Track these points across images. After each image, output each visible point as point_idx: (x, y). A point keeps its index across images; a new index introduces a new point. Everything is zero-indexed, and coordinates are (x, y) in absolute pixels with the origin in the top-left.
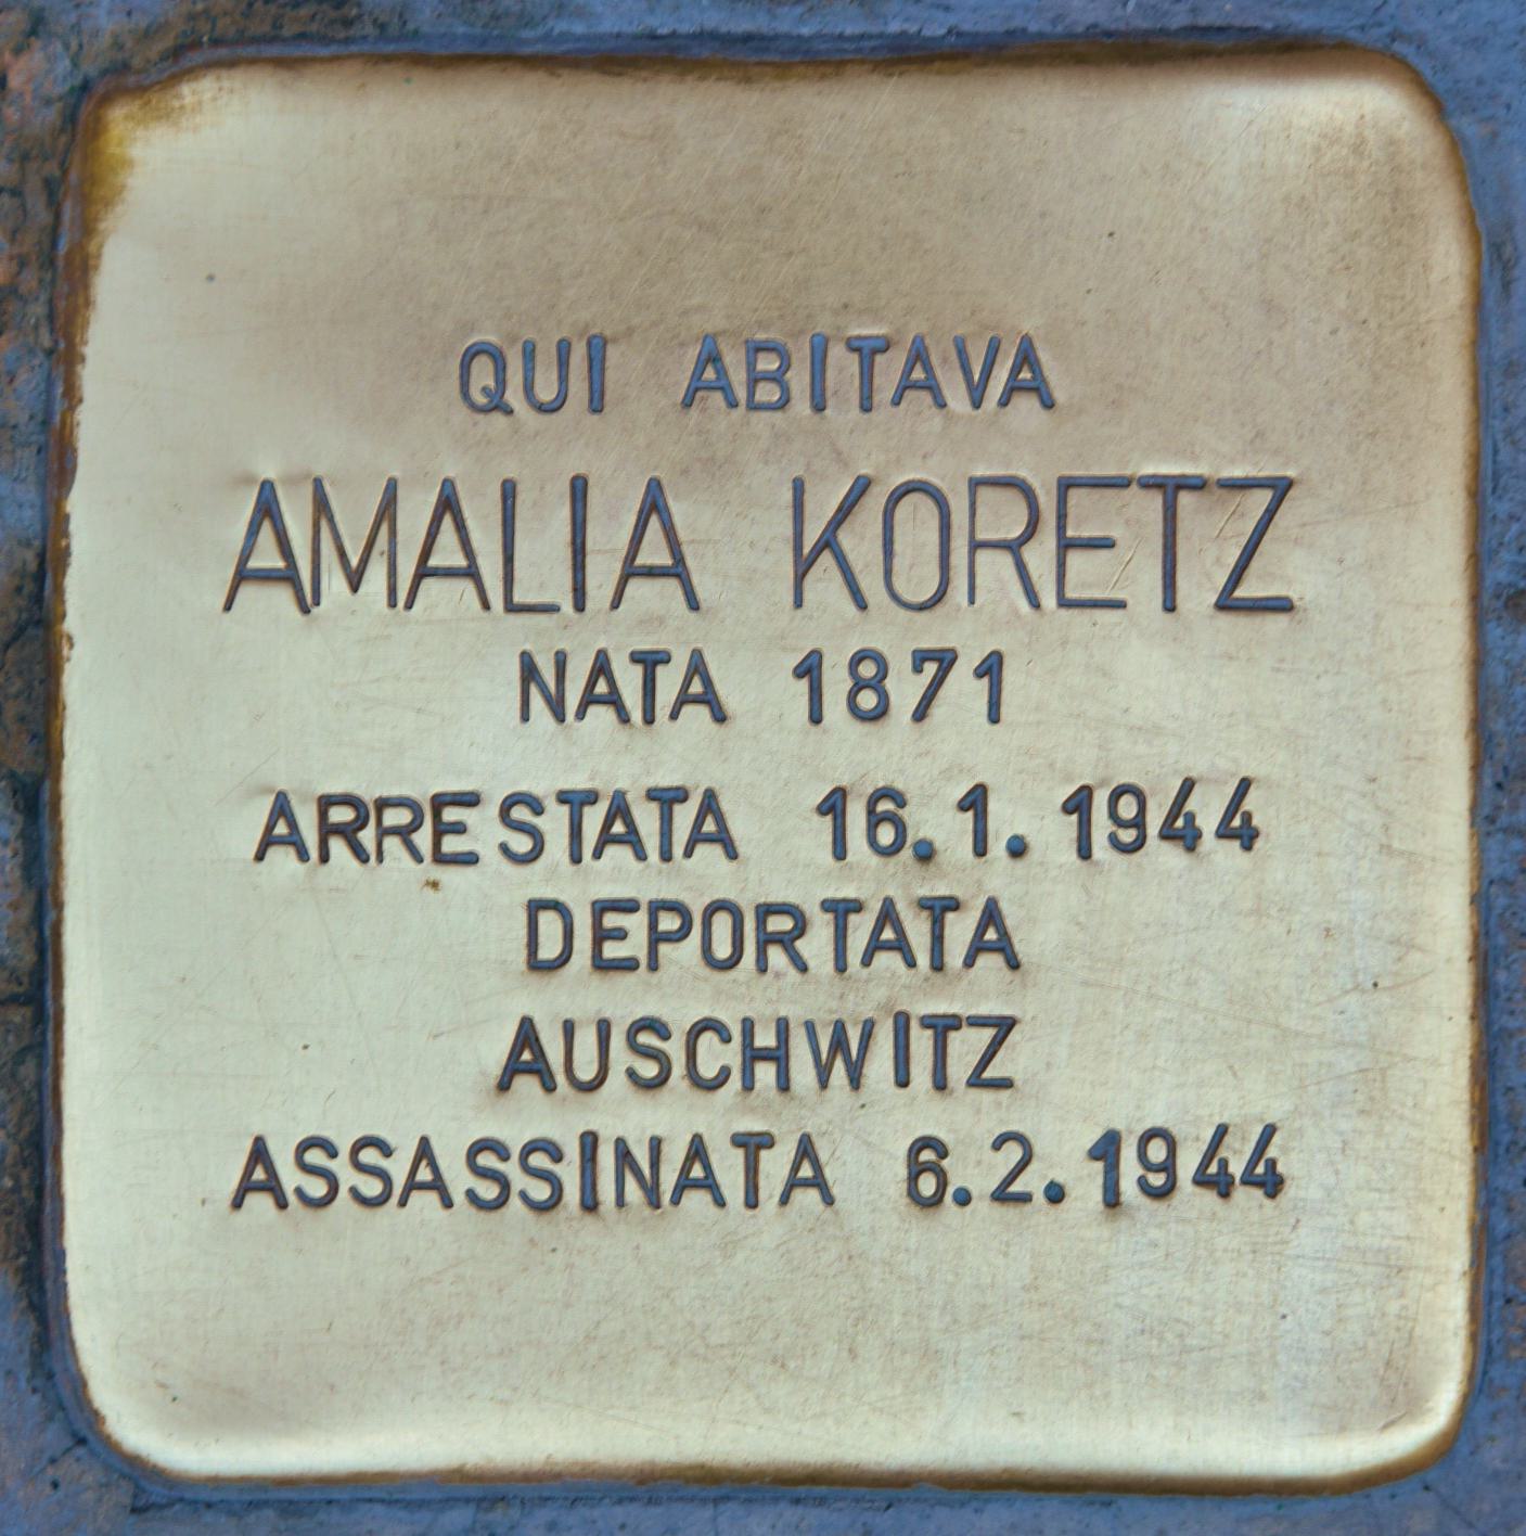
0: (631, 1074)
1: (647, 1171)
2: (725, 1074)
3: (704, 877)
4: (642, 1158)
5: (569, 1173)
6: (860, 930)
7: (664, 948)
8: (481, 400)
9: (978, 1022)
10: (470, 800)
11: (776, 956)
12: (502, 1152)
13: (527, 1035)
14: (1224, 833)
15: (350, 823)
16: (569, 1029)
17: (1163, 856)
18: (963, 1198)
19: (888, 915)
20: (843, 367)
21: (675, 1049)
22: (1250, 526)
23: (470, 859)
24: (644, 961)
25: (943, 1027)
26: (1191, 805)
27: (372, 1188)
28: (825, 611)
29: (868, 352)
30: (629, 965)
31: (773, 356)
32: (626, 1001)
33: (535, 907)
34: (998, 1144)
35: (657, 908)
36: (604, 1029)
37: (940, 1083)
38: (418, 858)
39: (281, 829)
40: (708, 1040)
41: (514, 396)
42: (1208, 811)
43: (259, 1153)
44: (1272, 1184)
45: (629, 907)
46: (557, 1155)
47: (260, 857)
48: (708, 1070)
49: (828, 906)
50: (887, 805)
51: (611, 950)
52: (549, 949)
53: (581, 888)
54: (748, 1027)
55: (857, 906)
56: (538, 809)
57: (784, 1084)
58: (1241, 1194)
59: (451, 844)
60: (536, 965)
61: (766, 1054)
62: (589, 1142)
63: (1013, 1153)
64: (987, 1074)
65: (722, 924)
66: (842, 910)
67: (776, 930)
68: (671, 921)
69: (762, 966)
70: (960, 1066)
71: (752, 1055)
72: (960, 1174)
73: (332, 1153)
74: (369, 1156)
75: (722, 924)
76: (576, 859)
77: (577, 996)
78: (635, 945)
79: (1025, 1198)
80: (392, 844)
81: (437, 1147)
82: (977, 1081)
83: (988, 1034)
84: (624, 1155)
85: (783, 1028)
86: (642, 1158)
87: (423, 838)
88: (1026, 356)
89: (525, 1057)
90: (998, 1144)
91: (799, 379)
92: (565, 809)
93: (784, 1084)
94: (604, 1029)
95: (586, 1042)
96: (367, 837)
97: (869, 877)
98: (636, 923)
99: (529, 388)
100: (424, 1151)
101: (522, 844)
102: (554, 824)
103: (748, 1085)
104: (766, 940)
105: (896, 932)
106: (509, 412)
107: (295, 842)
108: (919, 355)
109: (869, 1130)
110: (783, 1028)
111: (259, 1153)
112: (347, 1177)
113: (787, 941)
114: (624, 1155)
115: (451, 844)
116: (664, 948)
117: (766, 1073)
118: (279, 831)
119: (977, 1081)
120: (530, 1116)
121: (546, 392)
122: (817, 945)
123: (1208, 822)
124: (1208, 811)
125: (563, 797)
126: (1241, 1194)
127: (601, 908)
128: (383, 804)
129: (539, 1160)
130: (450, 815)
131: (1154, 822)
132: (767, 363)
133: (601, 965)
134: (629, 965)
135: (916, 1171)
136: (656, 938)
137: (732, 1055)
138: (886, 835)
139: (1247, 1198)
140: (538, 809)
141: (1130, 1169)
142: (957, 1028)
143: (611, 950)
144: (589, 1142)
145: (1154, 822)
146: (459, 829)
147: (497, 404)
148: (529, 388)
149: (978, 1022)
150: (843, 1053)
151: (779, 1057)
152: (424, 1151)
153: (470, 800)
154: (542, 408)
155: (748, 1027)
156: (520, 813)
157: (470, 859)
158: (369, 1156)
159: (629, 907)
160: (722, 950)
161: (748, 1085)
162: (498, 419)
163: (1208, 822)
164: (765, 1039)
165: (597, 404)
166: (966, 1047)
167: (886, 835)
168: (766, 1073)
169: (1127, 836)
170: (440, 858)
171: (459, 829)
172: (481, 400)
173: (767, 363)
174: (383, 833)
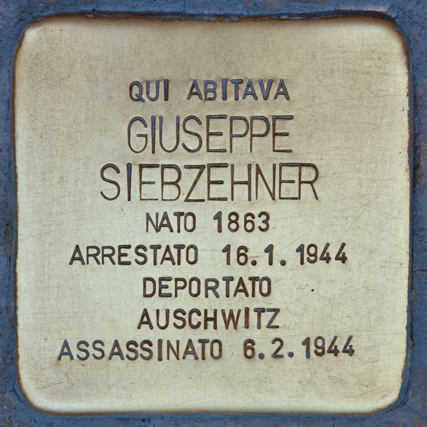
0: (175, 325)
1: (175, 349)
2: (199, 324)
3: (185, 271)
4: (174, 346)
5: (155, 349)
6: (233, 285)
7: (179, 291)
8: (135, 97)
9: (269, 310)
10: (129, 247)
11: (210, 292)
12: (135, 344)
13: (145, 313)
14: (337, 258)
15: (99, 254)
16: (158, 312)
17: (321, 263)
18: (262, 356)
19: (241, 281)
20: (231, 88)
21: (186, 317)
22: (267, 181)
23: (128, 263)
24: (173, 295)
25: (260, 311)
26: (328, 250)
27: (99, 354)
28: (118, 218)
29: (237, 83)
30: (169, 295)
31: (212, 85)
32: (172, 305)
33: (146, 279)
34: (274, 341)
35: (177, 280)
36: (167, 312)
37: (259, 327)
38: (114, 263)
39: (77, 255)
40: (194, 315)
41: (144, 96)
42: (333, 252)
43: (66, 344)
44: (351, 352)
45: (169, 279)
46: (150, 344)
47: (71, 263)
48: (195, 323)
49: (224, 279)
50: (243, 251)
51: (164, 291)
52: (149, 291)
53: (156, 273)
54: (206, 311)
55: (232, 279)
56: (145, 250)
57: (215, 327)
58: (341, 355)
59: (123, 259)
60: (145, 296)
61: (210, 319)
62: (160, 342)
63: (278, 344)
64: (272, 324)
65: (194, 283)
66: (228, 280)
67: (211, 286)
68: (183, 283)
69: (207, 296)
70: (264, 323)
71: (207, 319)
72: (258, 349)
73: (87, 345)
74: (98, 345)
75: (194, 283)
76: (155, 264)
77: (156, 304)
78: (171, 290)
79: (282, 356)
80: (107, 259)
81: (120, 343)
82: (269, 326)
83: (272, 313)
84: (169, 345)
85: (215, 312)
86: (174, 346)
87: (115, 258)
88: (282, 85)
89: (145, 319)
90: (274, 341)
91: (219, 91)
92: (153, 250)
93: (215, 327)
94: (167, 312)
95: (163, 315)
96: (99, 257)
97: (238, 272)
98: (171, 284)
99: (148, 93)
100: (116, 344)
101: (141, 259)
102: (150, 253)
103: (206, 328)
104: (207, 288)
105: (243, 287)
106: (143, 101)
107: (81, 259)
108: (250, 85)
109: (233, 340)
110: (215, 312)
111: (66, 344)
112: (91, 350)
113: (214, 289)
114: (169, 345)
115: (123, 259)
116: (179, 291)
117: (211, 324)
118: (77, 257)
119: (269, 326)
120: (145, 333)
121: (153, 95)
122: (221, 290)
123: (333, 256)
124: (333, 252)
125: (152, 247)
126: (341, 355)
127: (161, 279)
128: (104, 248)
129: (146, 346)
130: (123, 251)
131: (319, 255)
132: (211, 87)
133: (161, 295)
134: (169, 295)
135: (246, 348)
136: (177, 288)
137: (201, 319)
138: (242, 259)
139: (343, 356)
140: (145, 250)
141: (313, 348)
142: (264, 312)
143: (164, 291)
144: (160, 342)
145: (319, 255)
146: (125, 255)
147: (140, 99)
148: (148, 93)
149: (269, 310)
150: (231, 319)
151: (214, 319)
152: (116, 344)
153: (129, 247)
154: (152, 100)
155: (206, 311)
156: (141, 251)
157: (128, 263)
158: (98, 345)
159: (169, 279)
160: (194, 291)
161: (206, 328)
162: (141, 104)
163: (333, 256)
164: (210, 315)
165: (166, 99)
166: (266, 317)
167: (242, 259)
168: (211, 324)
169: (312, 258)
170: (121, 263)
171: (125, 255)
172: (135, 97)
173: (211, 87)
174: (104, 256)
